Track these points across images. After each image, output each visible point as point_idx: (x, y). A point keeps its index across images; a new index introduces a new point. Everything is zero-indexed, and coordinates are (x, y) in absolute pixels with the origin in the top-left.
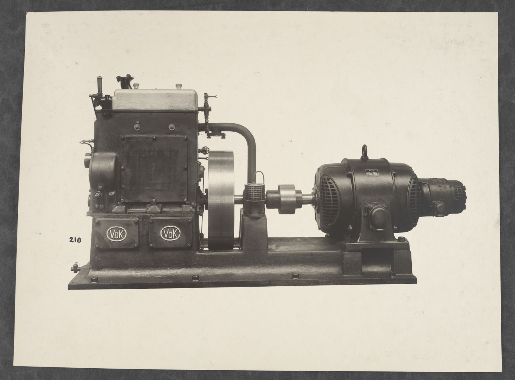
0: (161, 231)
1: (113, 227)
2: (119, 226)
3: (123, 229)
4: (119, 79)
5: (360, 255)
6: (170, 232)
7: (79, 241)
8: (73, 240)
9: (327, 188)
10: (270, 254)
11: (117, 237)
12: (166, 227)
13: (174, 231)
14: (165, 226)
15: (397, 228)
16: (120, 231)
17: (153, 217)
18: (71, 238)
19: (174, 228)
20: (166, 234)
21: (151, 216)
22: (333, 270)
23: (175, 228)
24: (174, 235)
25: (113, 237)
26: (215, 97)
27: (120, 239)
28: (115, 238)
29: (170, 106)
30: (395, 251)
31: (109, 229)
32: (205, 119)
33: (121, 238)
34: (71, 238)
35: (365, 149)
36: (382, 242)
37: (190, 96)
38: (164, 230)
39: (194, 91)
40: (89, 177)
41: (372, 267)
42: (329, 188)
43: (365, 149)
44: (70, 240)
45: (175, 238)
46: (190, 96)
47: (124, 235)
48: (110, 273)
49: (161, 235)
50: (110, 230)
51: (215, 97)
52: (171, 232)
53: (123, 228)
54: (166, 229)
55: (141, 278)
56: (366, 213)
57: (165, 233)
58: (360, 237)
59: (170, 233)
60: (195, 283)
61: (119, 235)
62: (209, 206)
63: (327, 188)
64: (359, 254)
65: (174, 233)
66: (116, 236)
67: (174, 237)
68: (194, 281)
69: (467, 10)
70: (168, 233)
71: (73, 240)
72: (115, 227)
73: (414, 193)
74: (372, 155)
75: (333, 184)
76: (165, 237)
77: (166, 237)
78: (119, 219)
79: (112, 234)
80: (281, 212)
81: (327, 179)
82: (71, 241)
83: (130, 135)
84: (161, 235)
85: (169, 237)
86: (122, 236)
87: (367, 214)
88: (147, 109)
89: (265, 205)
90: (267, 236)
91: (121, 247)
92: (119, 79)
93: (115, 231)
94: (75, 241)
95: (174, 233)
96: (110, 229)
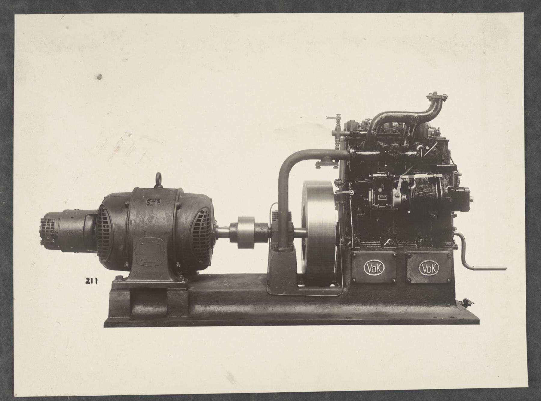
1: (373, 260)
3: (381, 263)
4: (444, 98)
7: (88, 279)
8: (89, 282)
11: (430, 271)
12: (376, 260)
13: (432, 265)
15: (181, 266)
18: (88, 279)
20: (425, 269)
23: (379, 262)
26: (328, 118)
27: (432, 273)
32: (336, 145)
34: (88, 279)
35: (159, 178)
40: (470, 207)
43: (159, 178)
44: (87, 280)
45: (434, 273)
50: (367, 264)
51: (328, 118)
53: (380, 262)
55: (400, 314)
61: (377, 270)
65: (433, 268)
66: (429, 271)
67: (432, 272)
69: (130, 10)
71: (89, 282)
73: (199, 224)
74: (166, 184)
75: (108, 220)
76: (423, 272)
77: (370, 272)
79: (370, 268)
80: (240, 247)
82: (87, 283)
85: (373, 272)
86: (379, 270)
90: (297, 272)
92: (444, 98)
94: (92, 279)
95: (378, 268)
96: (367, 263)
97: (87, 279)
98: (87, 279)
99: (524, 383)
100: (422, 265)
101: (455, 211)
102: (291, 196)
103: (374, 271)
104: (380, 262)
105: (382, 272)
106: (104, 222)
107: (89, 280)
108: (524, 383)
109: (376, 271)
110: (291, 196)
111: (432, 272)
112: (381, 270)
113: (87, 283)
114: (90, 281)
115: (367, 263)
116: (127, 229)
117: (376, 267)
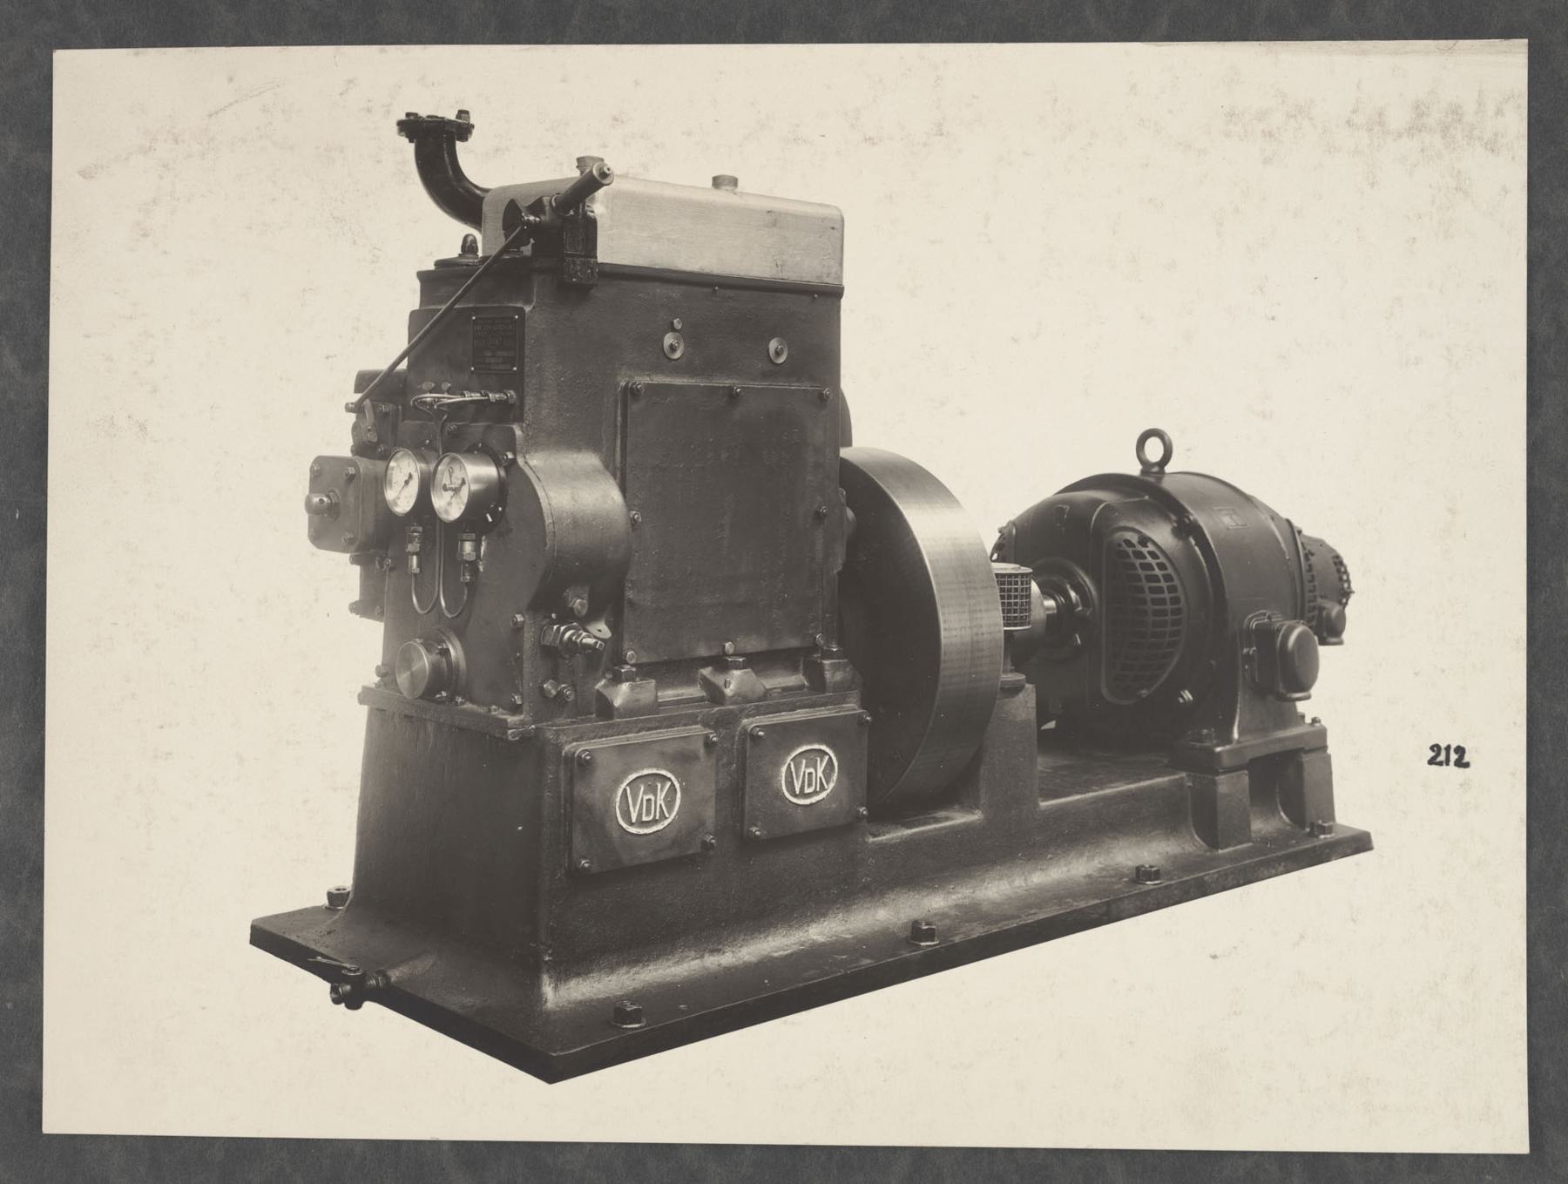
0: (784, 769)
1: (638, 775)
2: (657, 767)
3: (669, 779)
5: (1246, 779)
6: (648, 797)
9: (1150, 573)
10: (1045, 811)
14: (793, 749)
16: (659, 786)
17: (748, 716)
18: (1436, 748)
19: (820, 750)
21: (742, 711)
22: (1152, 851)
24: (820, 778)
25: (800, 792)
28: (645, 819)
29: (777, 265)
30: (1305, 758)
31: (673, 778)
33: (663, 817)
34: (1436, 748)
36: (1281, 734)
37: (833, 228)
38: (628, 789)
39: (839, 210)
41: (883, 903)
42: (1157, 571)
44: (1433, 754)
46: (833, 228)
47: (670, 804)
48: (870, 918)
49: (784, 788)
50: (628, 789)
52: (812, 770)
53: (669, 775)
54: (798, 760)
56: (1252, 647)
57: (796, 773)
58: (1237, 723)
59: (810, 774)
60: (636, 1036)
62: (945, 646)
63: (1150, 573)
64: (1245, 778)
66: (648, 813)
67: (818, 790)
68: (1322, 837)
70: (804, 772)
72: (646, 772)
77: (634, 820)
78: (653, 736)
79: (634, 805)
81: (1139, 542)
82: (1432, 762)
83: (649, 375)
84: (784, 788)
87: (1255, 648)
88: (707, 270)
89: (1077, 636)
91: (662, 856)
93: (806, 763)
96: (628, 785)
97: (1432, 748)
98: (1432, 748)
99: (1511, 1136)
100: (625, 790)
101: (450, 122)
102: (1093, 178)
103: (648, 813)
104: (669, 775)
105: (672, 817)
106: (1150, 588)
107: (1438, 754)
108: (1511, 1136)
109: (655, 816)
110: (1093, 178)
111: (818, 790)
112: (670, 810)
113: (1432, 762)
114: (1442, 757)
115: (625, 784)
116: (1298, 582)
117: (816, 772)
